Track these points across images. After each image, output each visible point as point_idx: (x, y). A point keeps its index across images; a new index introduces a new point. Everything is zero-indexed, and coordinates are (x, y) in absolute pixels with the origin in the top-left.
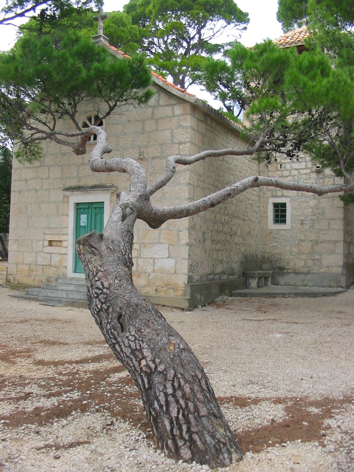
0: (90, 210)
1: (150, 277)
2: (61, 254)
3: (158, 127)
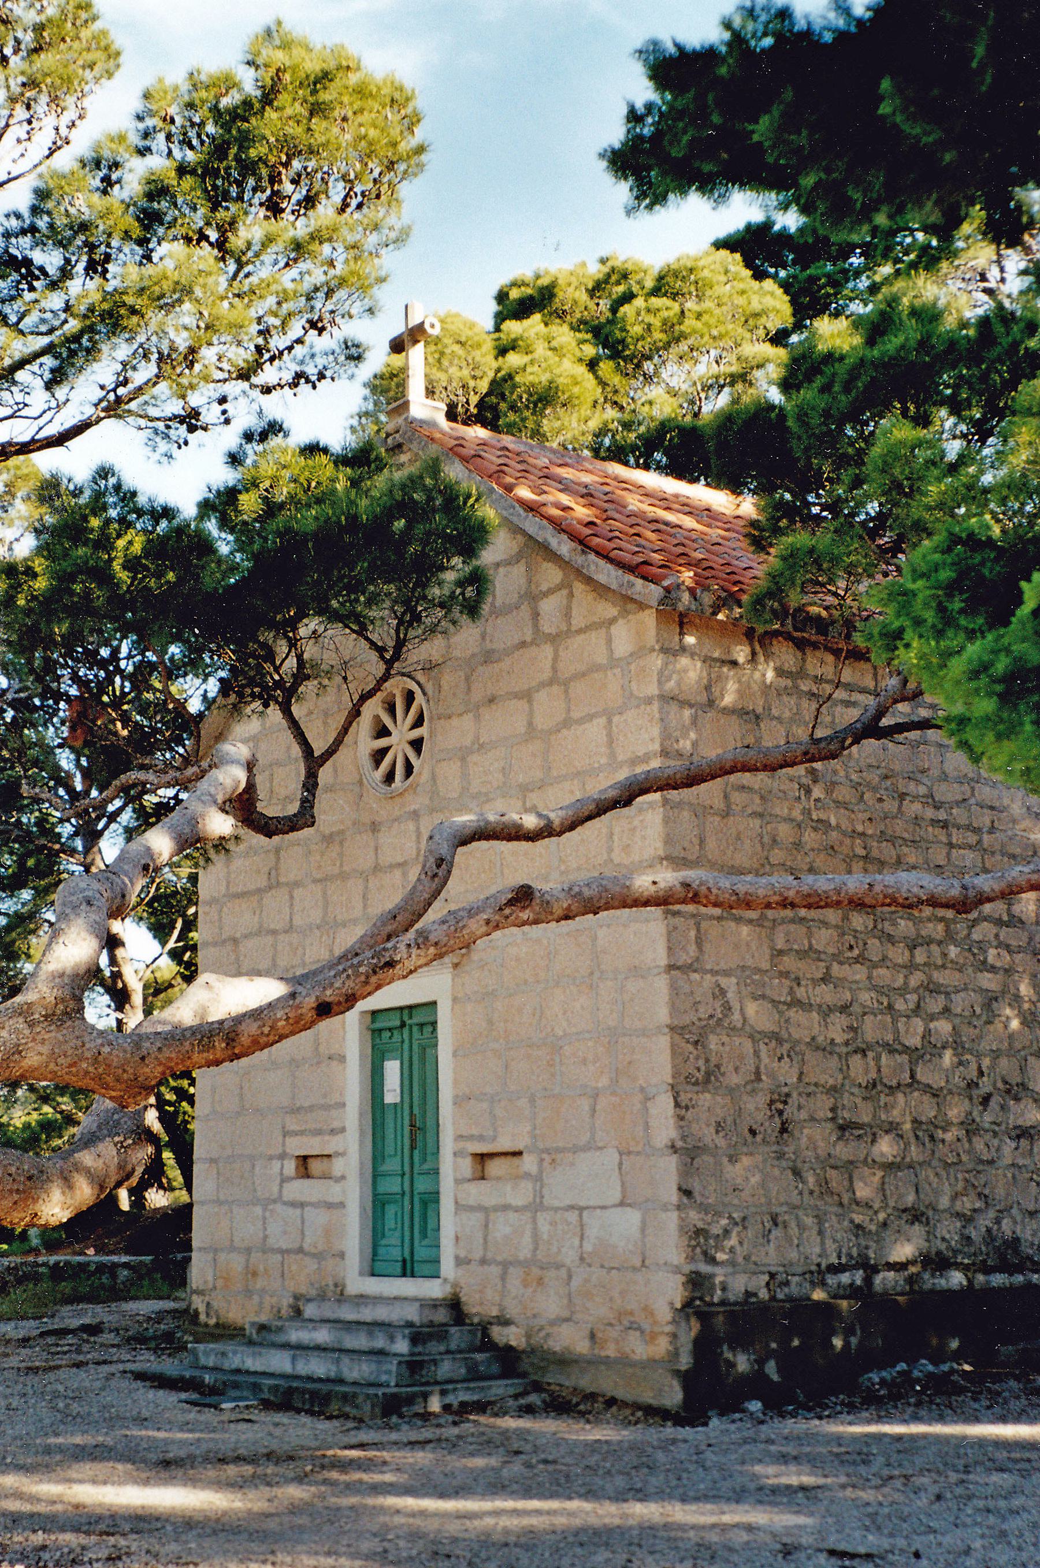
0: (406, 1031)
1: (575, 1283)
2: (330, 1206)
3: (569, 710)
